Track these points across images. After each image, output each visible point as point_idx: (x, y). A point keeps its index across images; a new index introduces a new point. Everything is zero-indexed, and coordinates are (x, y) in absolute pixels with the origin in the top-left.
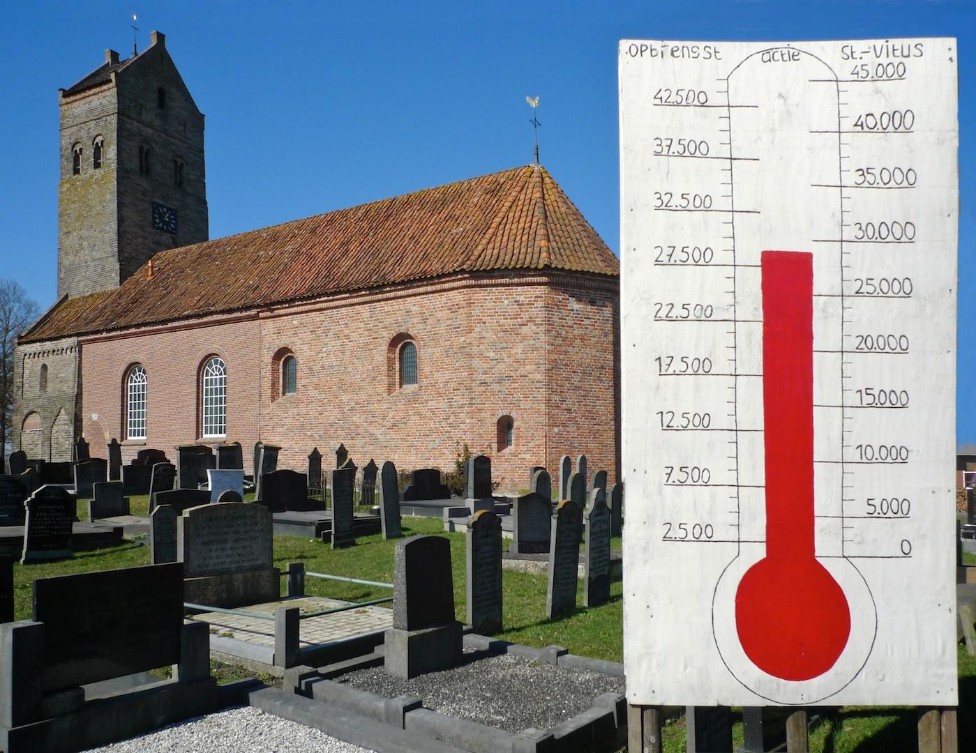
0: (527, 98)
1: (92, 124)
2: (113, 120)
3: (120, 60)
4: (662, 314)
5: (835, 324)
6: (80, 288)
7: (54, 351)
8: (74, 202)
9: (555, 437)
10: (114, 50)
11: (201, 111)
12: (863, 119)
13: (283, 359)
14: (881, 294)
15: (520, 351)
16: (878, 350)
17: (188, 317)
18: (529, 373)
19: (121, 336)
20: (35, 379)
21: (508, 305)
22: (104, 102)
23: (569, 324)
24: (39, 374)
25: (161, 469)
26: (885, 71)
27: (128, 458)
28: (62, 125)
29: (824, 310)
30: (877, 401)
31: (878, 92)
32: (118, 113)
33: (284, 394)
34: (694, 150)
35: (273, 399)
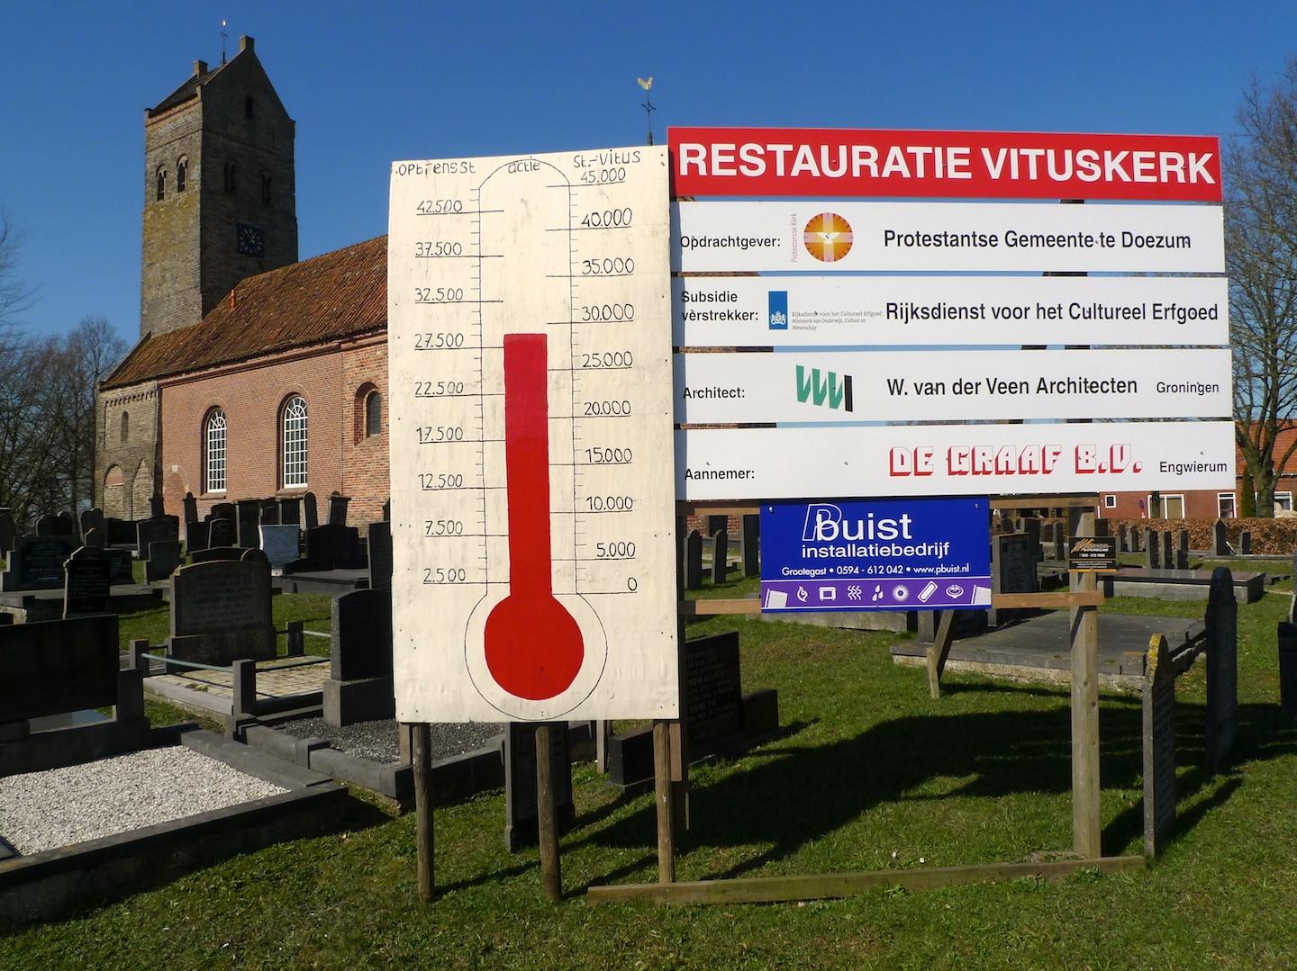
0: (639, 79)
1: (177, 144)
2: (198, 137)
3: (209, 70)
4: (422, 391)
5: (566, 393)
6: (163, 325)
7: (134, 397)
8: (158, 231)
10: (202, 60)
12: (589, 218)
13: (367, 396)
14: (605, 366)
16: (604, 414)
17: (267, 353)
19: (200, 377)
20: (117, 428)
22: (189, 118)
24: (120, 423)
25: (219, 525)
26: (608, 176)
27: (203, 513)
28: (147, 147)
29: (557, 383)
30: (604, 458)
31: (602, 193)
32: (203, 130)
33: (368, 436)
34: (449, 251)
35: (356, 442)
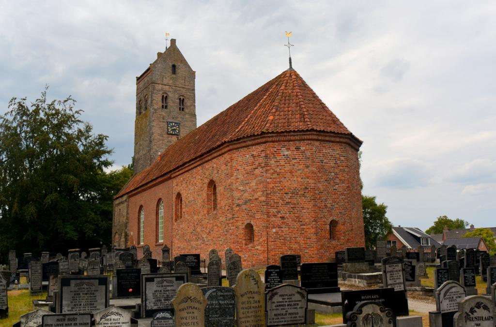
9: (273, 235)
11: (194, 70)
15: (254, 184)
18: (259, 197)
21: (249, 158)
23: (282, 164)
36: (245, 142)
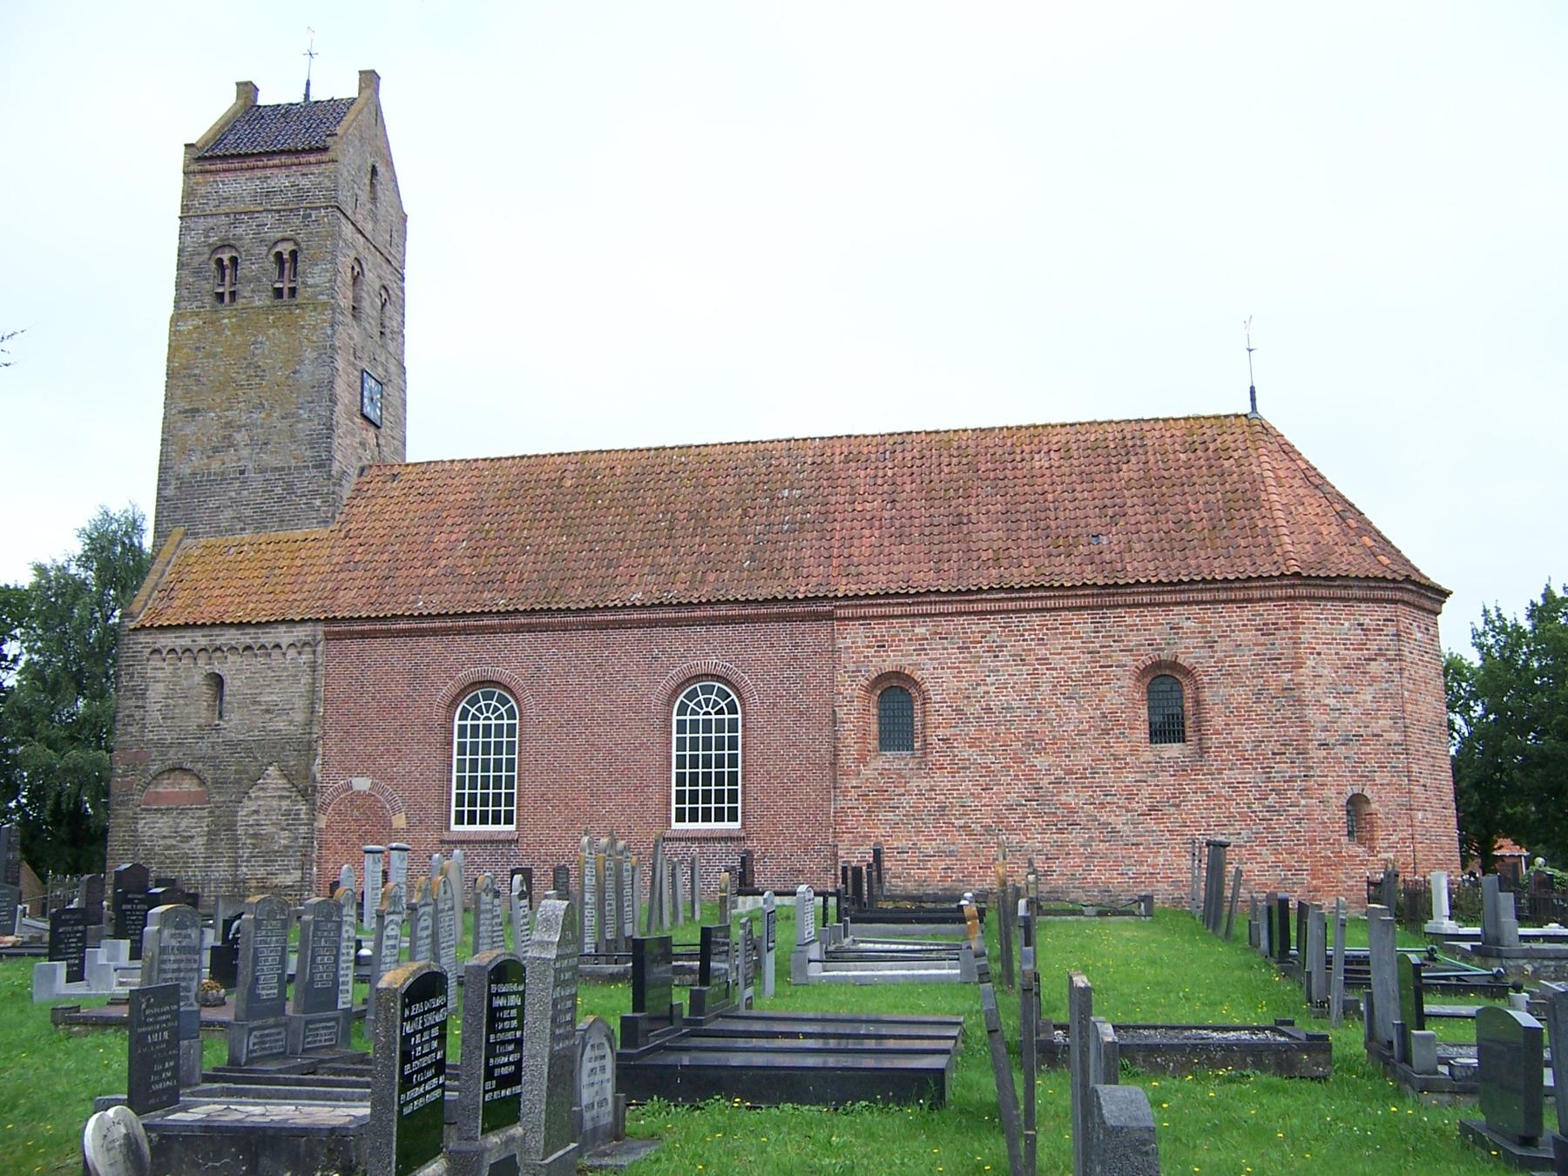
15: (1369, 697)
36: (1346, 587)
